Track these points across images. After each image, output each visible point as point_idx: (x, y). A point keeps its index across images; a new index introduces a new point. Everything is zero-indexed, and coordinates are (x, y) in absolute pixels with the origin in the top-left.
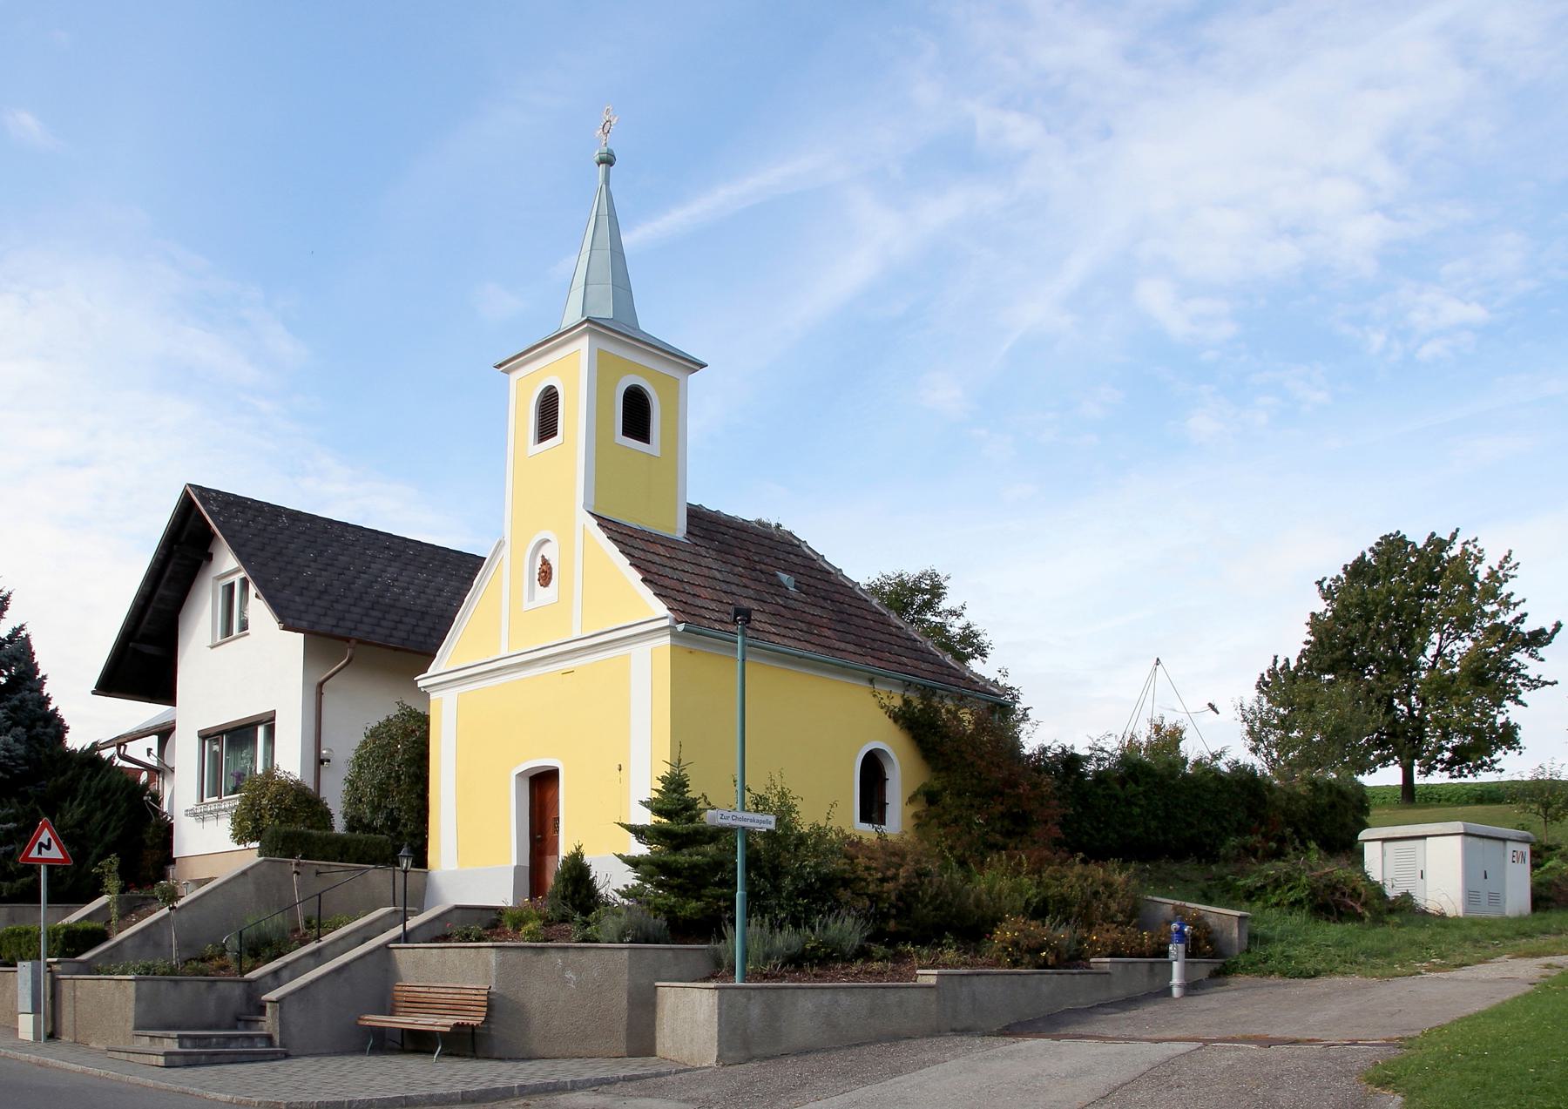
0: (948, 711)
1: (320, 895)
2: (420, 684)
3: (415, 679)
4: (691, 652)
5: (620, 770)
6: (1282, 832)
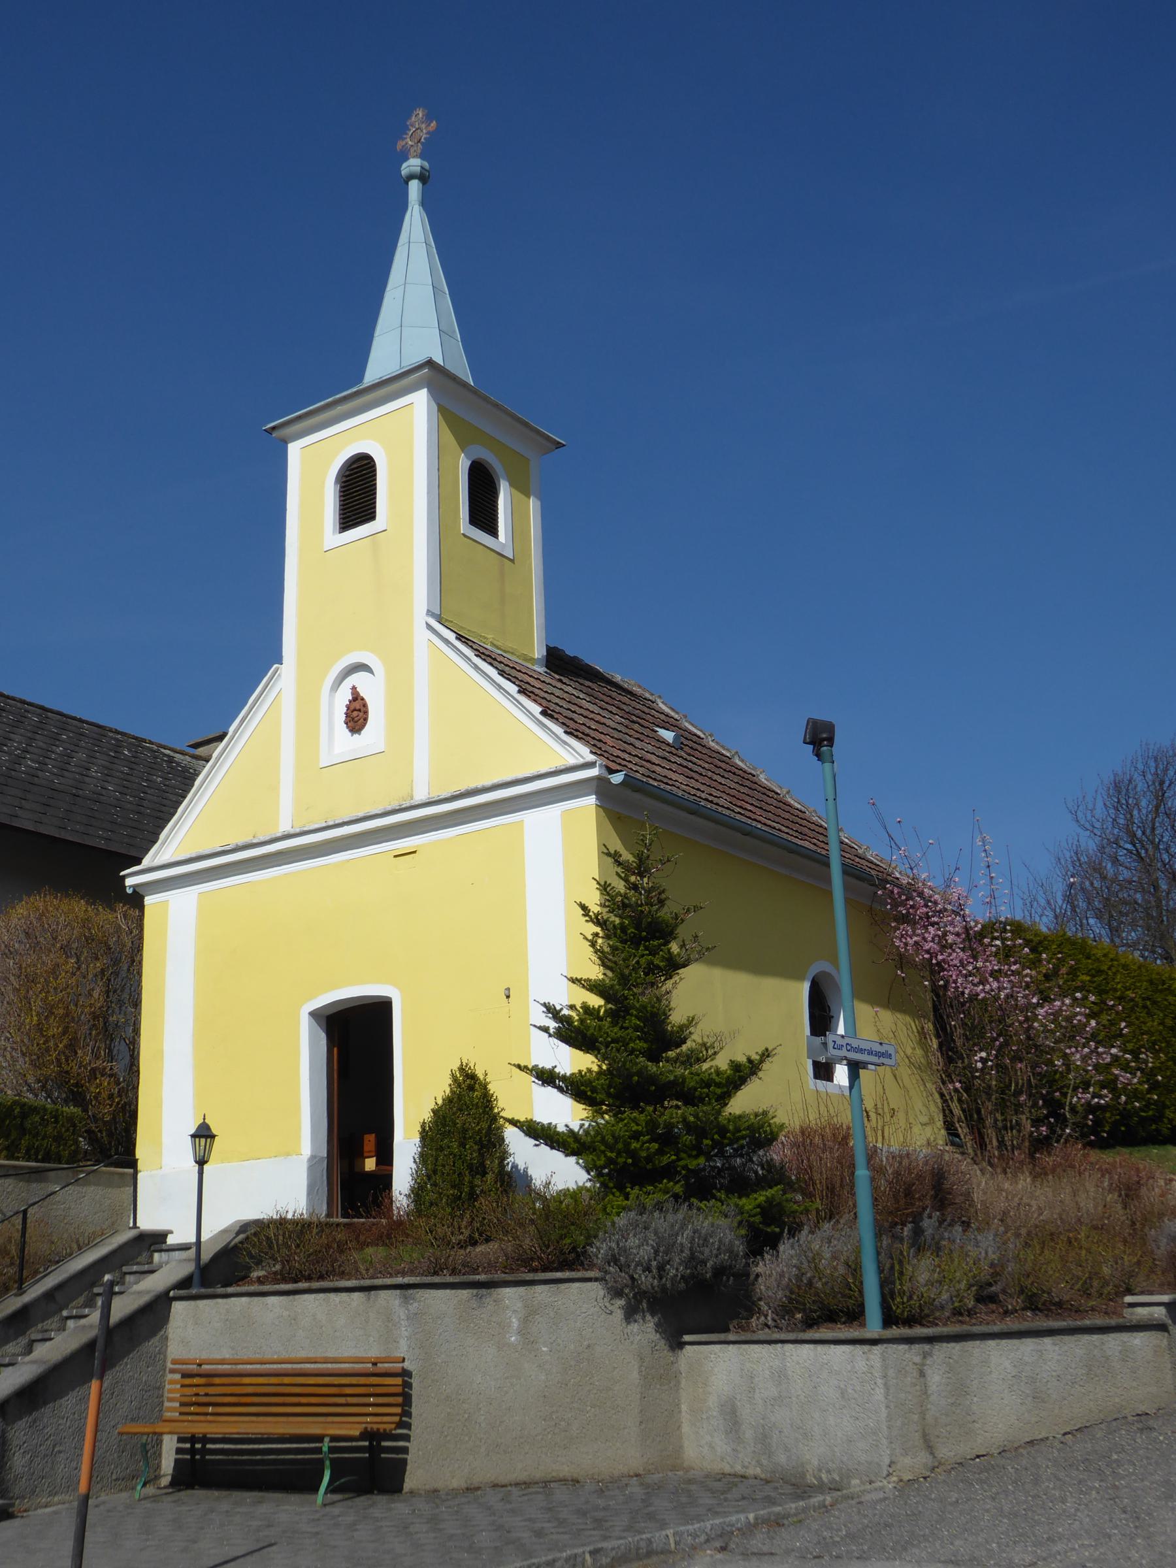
0: (58, 1029)
1: (25, 1212)
2: (129, 882)
3: (122, 873)
4: (619, 818)
5: (508, 997)
6: (408, 1310)
